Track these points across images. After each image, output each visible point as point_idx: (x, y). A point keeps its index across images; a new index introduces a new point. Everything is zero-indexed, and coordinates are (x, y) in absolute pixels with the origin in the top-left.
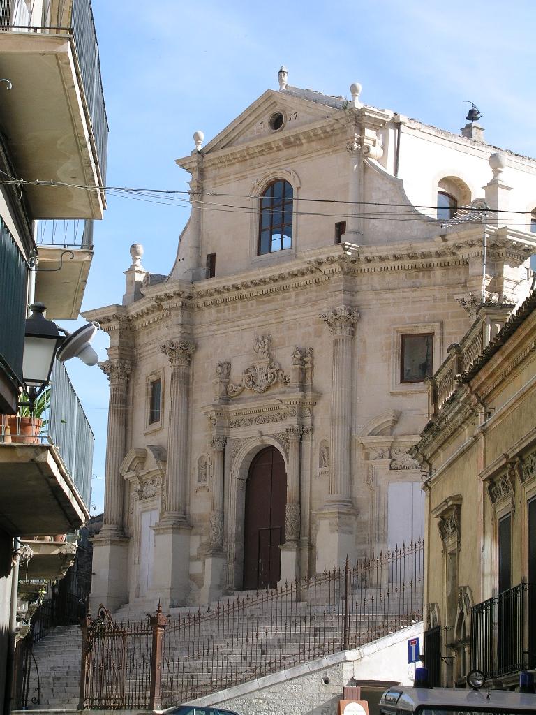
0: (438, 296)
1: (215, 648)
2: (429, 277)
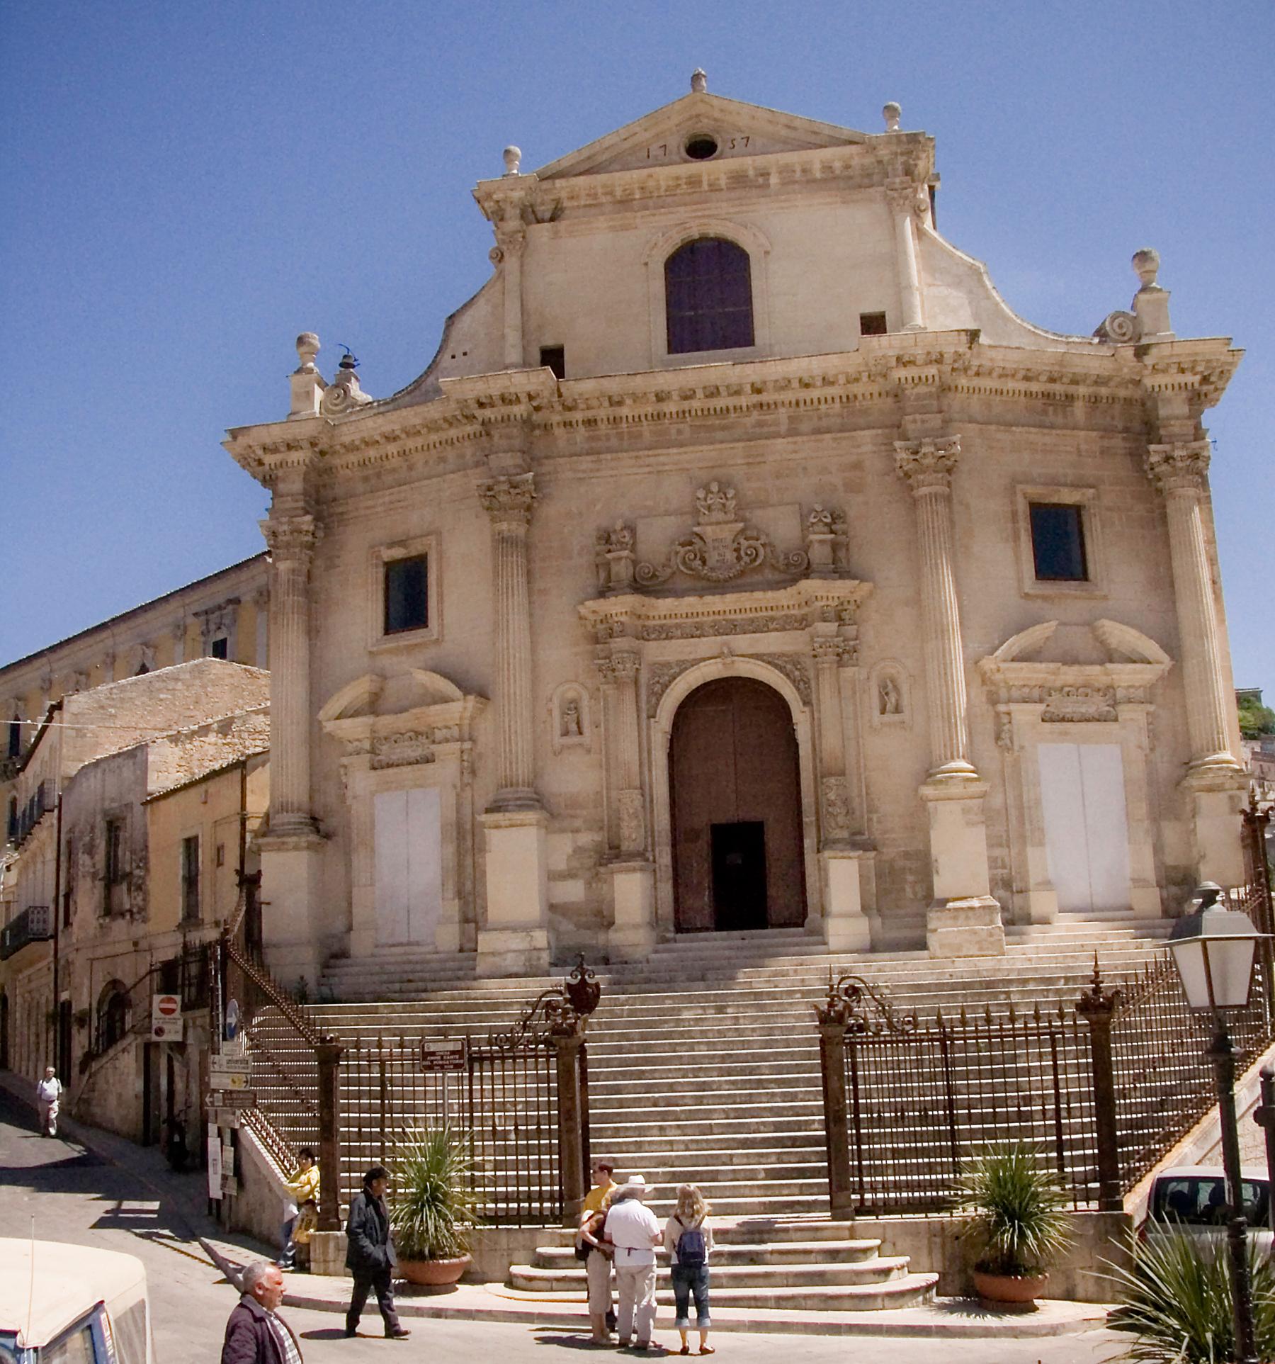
1: (477, 1095)
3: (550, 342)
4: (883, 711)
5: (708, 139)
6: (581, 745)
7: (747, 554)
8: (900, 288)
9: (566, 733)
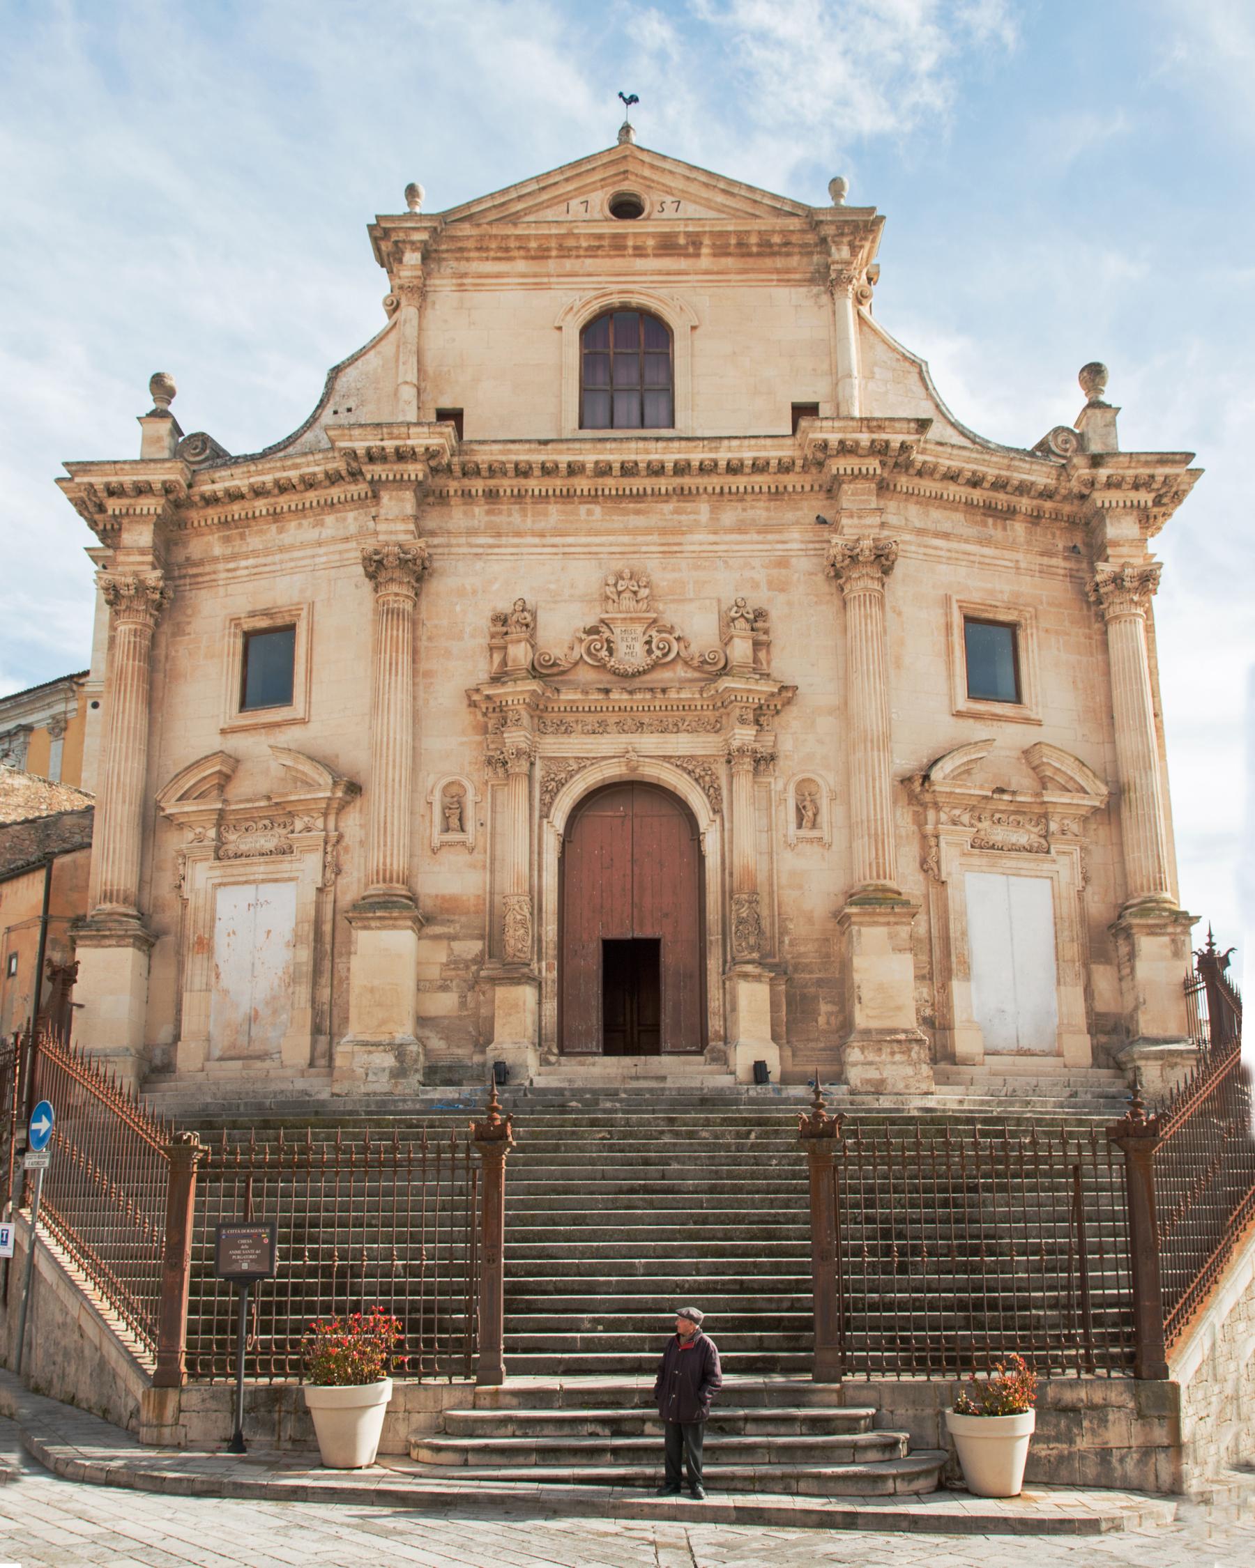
0: (1023, 565)
2: (1005, 529)
3: (447, 403)
4: (800, 826)
5: (634, 199)
6: (463, 844)
7: (658, 648)
8: (837, 376)
9: (447, 829)
